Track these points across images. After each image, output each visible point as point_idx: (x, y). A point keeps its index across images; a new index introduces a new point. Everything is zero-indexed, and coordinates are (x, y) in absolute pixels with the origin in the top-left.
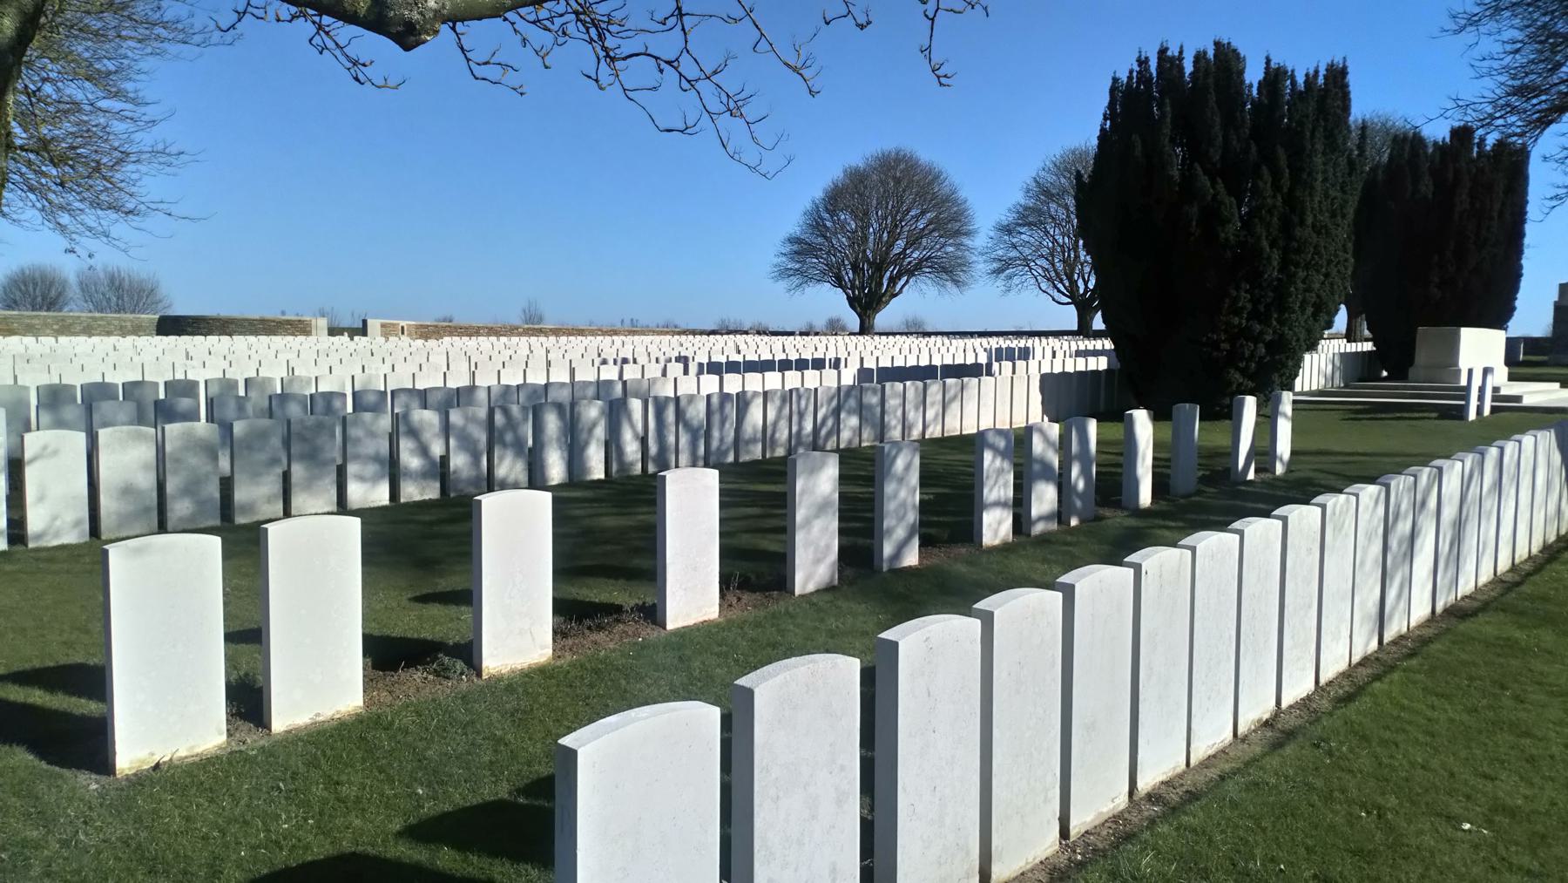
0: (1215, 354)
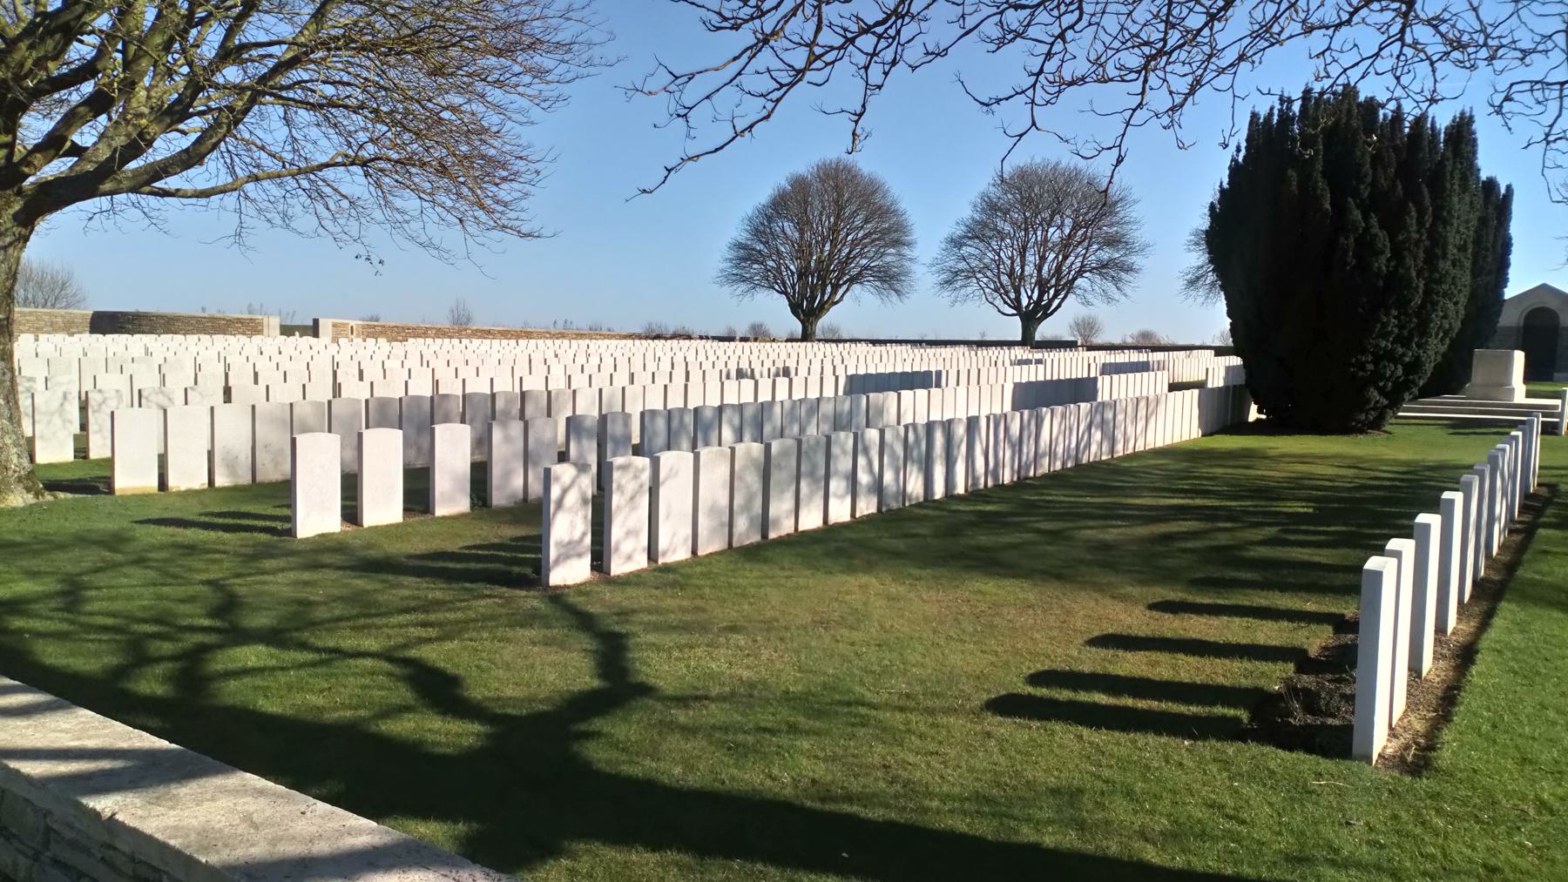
0: (1361, 373)
